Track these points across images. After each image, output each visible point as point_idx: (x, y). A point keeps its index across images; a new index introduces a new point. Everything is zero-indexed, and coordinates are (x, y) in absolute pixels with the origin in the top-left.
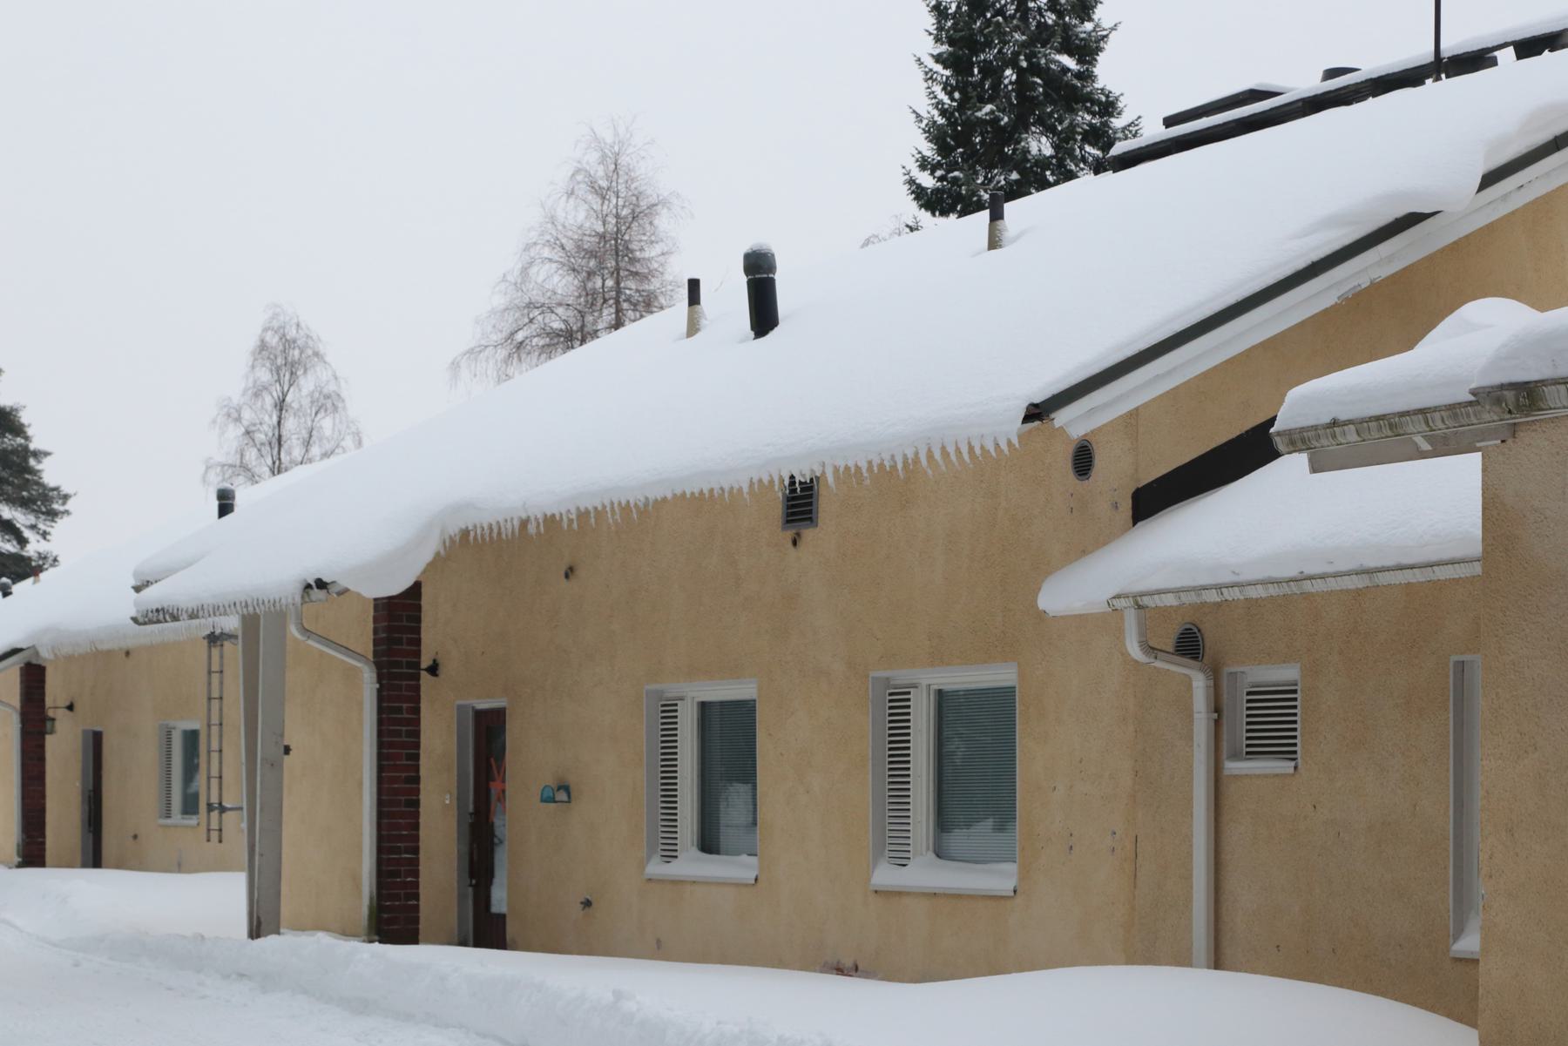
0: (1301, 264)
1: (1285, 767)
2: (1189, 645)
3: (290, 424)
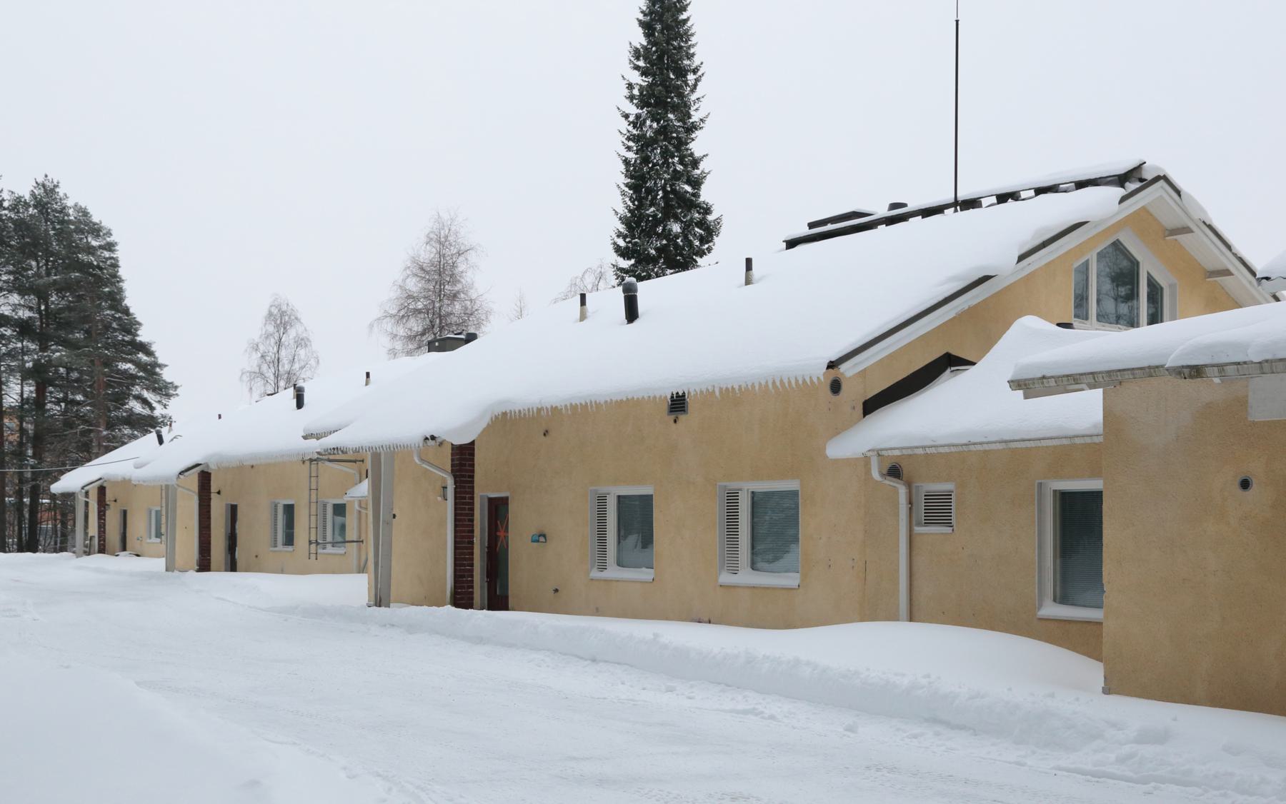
0: (941, 298)
1: (948, 530)
2: (894, 472)
3: (283, 353)
